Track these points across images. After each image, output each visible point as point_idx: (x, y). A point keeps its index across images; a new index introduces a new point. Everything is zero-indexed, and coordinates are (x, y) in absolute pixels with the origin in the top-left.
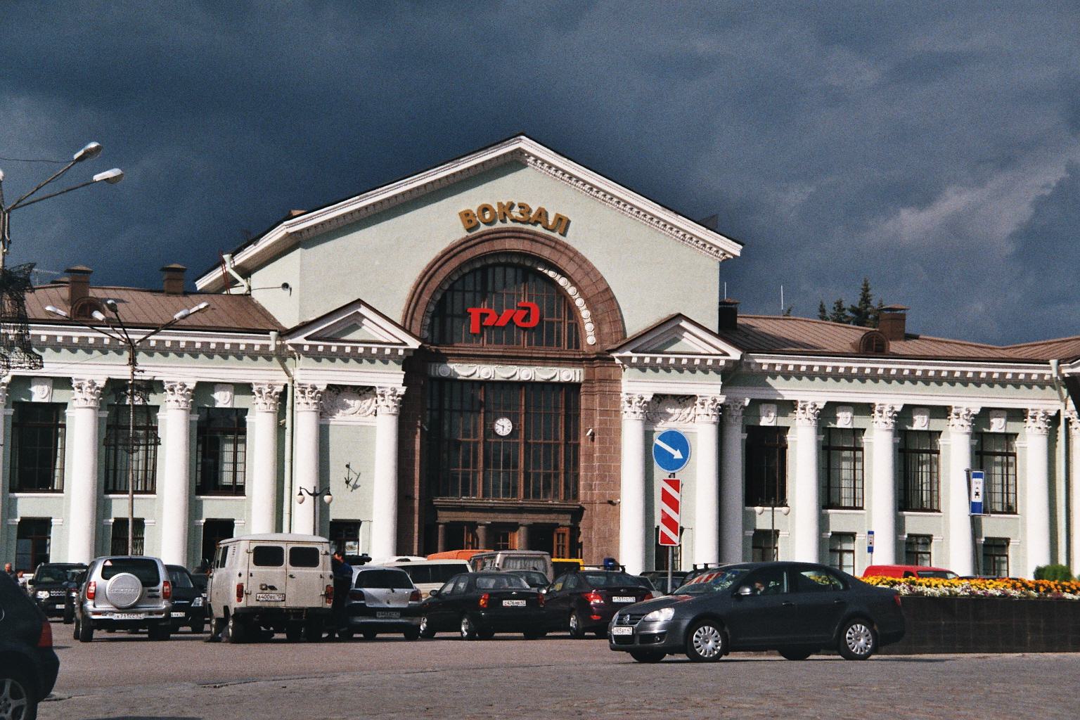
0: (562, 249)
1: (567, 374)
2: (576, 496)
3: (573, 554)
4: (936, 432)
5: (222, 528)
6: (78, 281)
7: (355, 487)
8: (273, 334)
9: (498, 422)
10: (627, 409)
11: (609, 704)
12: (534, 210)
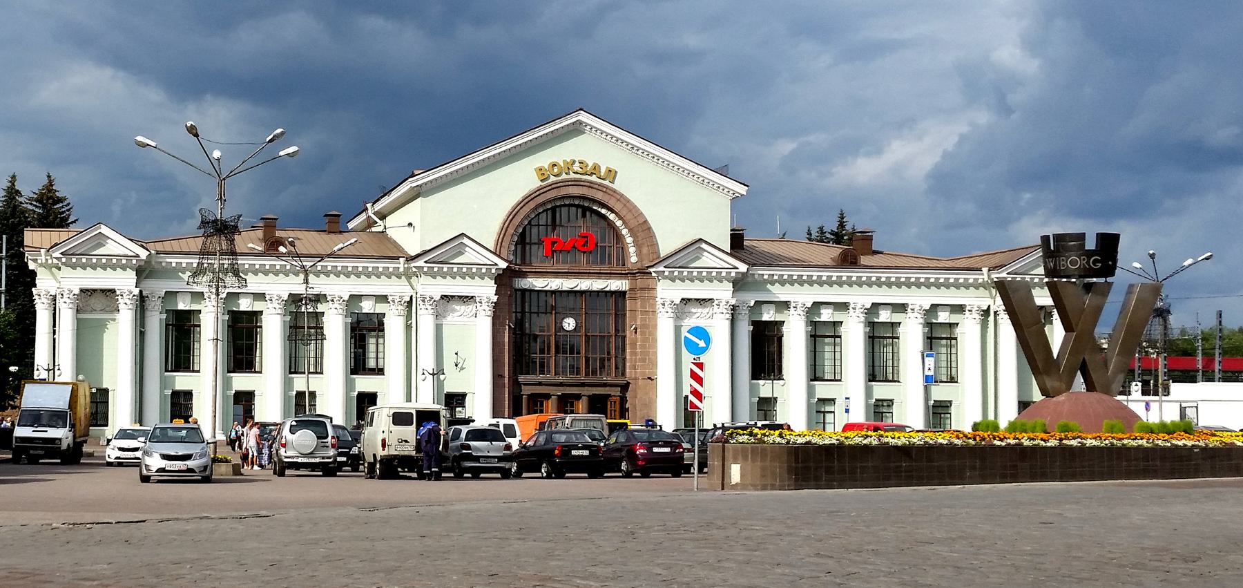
0: (612, 193)
1: (616, 285)
2: (623, 374)
3: (622, 416)
4: (954, 324)
5: (366, 401)
6: (269, 225)
7: (462, 369)
8: (402, 260)
9: (565, 320)
10: (661, 309)
11: (654, 526)
12: (590, 165)
